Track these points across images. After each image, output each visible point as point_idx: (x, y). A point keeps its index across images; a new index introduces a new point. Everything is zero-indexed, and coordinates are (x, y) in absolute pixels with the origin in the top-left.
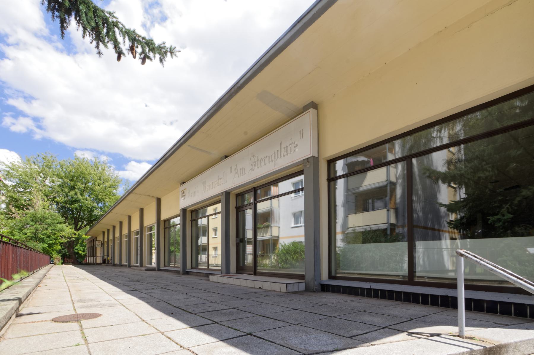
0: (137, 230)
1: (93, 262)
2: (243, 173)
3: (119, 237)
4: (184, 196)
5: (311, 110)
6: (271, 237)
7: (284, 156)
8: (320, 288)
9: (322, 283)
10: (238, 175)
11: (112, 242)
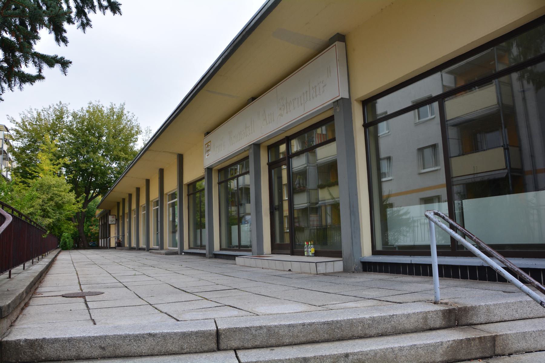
1: (107, 246)
2: (271, 120)
3: (136, 210)
4: (209, 150)
5: (336, 43)
7: (313, 98)
8: (360, 268)
9: (363, 261)
10: (267, 122)
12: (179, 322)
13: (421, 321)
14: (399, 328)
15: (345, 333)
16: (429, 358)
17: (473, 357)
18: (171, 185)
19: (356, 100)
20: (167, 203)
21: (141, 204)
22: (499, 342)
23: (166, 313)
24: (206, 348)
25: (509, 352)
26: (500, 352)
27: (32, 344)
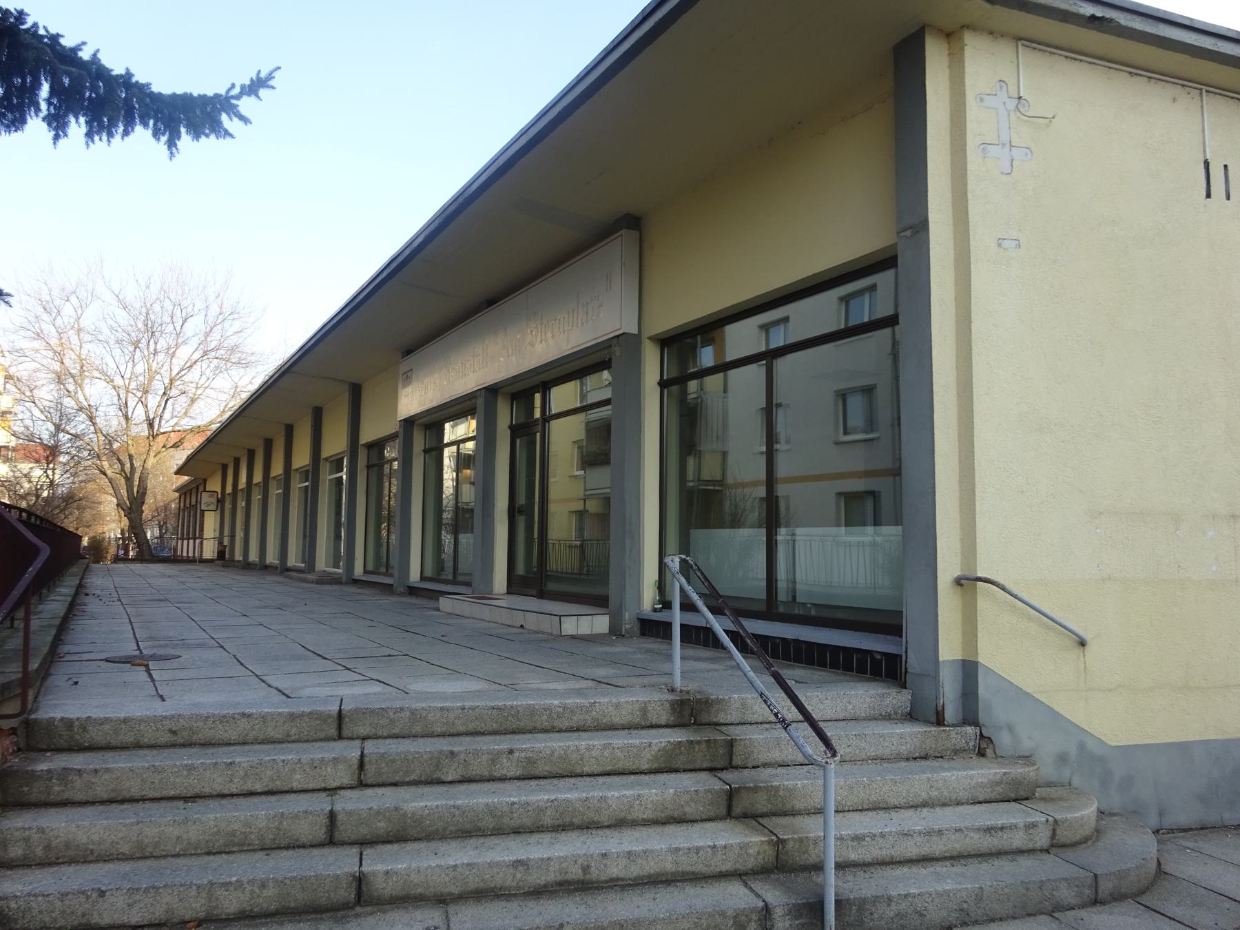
0: (304, 467)
6: (696, 484)
11: (245, 498)
12: (289, 700)
13: (638, 713)
14: (604, 721)
15: (522, 724)
16: (631, 763)
17: (697, 766)
18: (335, 442)
19: (650, 338)
20: (327, 477)
21: (273, 474)
22: (738, 749)
23: (276, 688)
24: (322, 735)
25: (755, 763)
26: (740, 763)
27: (68, 723)
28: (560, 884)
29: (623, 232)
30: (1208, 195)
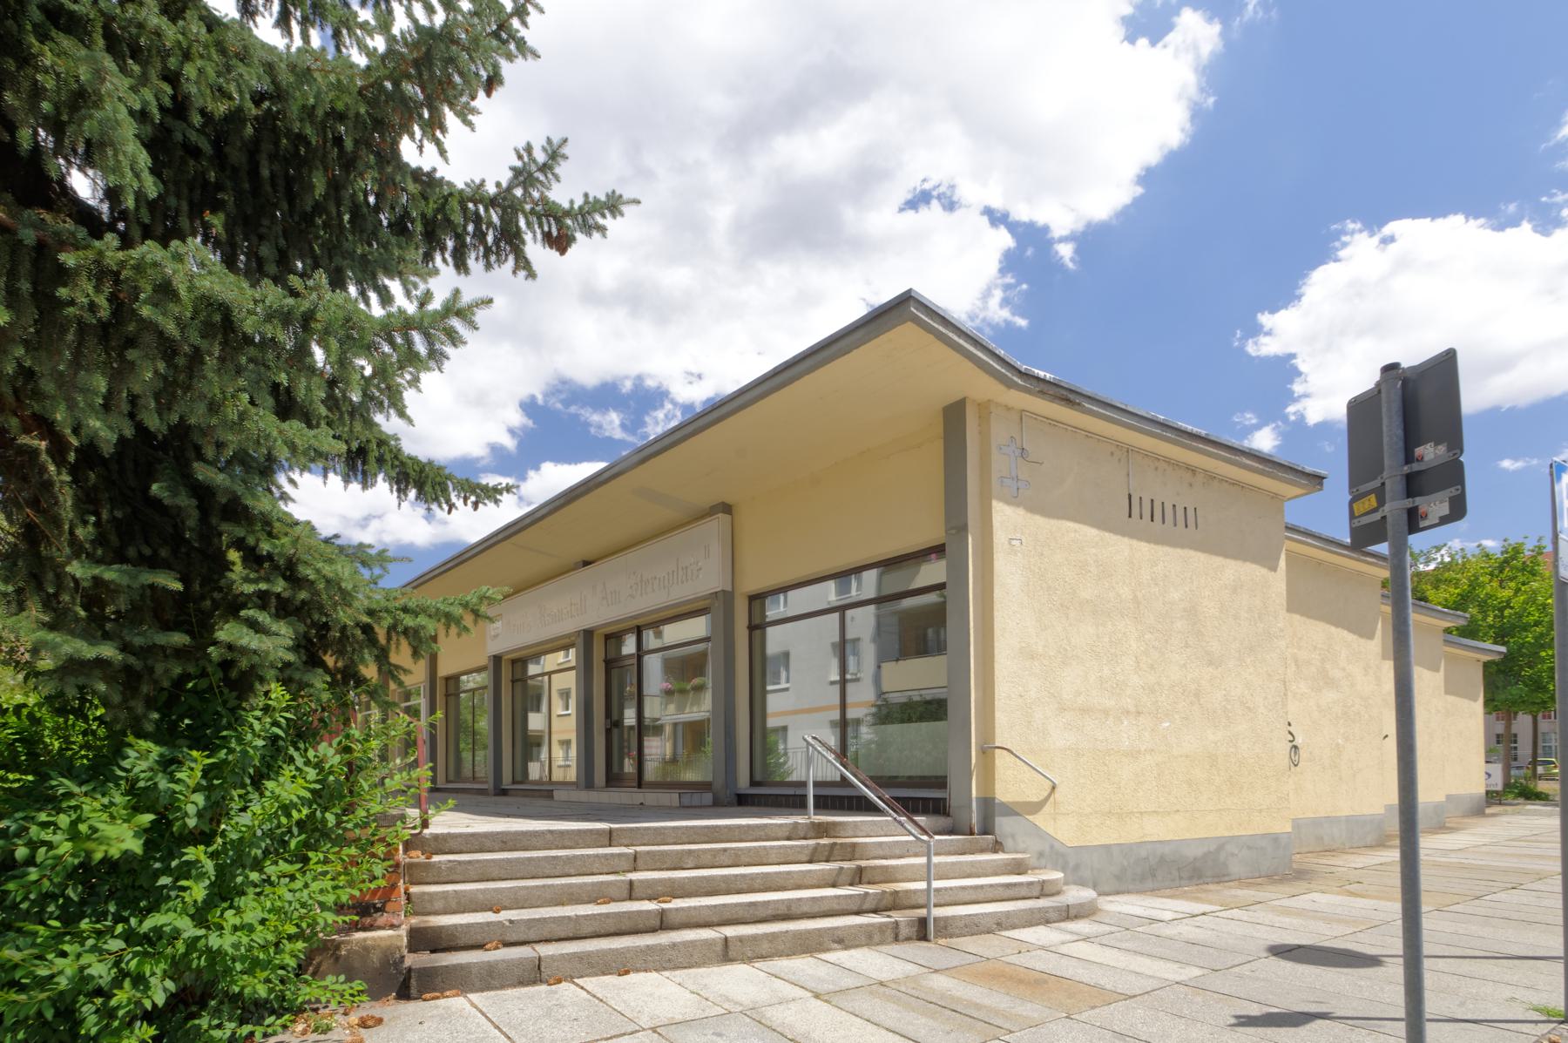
7: (682, 582)
28: (774, 916)
29: (720, 515)
30: (1130, 516)
